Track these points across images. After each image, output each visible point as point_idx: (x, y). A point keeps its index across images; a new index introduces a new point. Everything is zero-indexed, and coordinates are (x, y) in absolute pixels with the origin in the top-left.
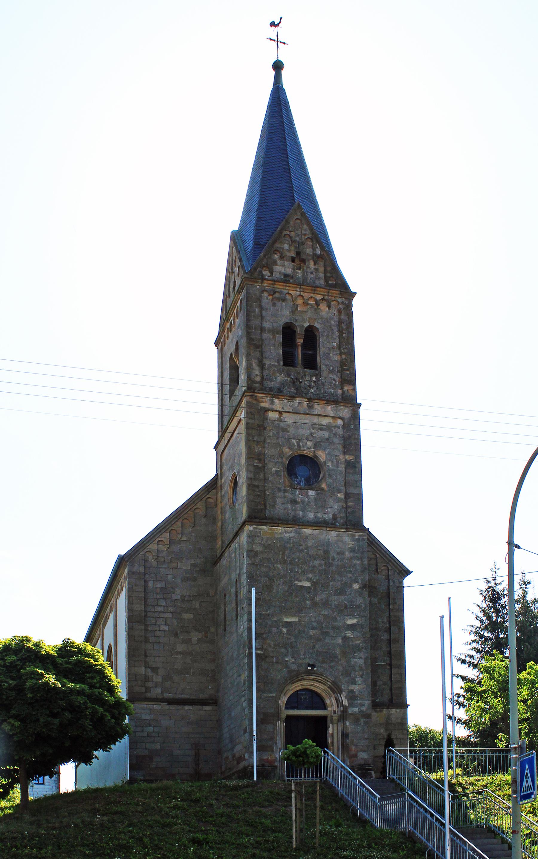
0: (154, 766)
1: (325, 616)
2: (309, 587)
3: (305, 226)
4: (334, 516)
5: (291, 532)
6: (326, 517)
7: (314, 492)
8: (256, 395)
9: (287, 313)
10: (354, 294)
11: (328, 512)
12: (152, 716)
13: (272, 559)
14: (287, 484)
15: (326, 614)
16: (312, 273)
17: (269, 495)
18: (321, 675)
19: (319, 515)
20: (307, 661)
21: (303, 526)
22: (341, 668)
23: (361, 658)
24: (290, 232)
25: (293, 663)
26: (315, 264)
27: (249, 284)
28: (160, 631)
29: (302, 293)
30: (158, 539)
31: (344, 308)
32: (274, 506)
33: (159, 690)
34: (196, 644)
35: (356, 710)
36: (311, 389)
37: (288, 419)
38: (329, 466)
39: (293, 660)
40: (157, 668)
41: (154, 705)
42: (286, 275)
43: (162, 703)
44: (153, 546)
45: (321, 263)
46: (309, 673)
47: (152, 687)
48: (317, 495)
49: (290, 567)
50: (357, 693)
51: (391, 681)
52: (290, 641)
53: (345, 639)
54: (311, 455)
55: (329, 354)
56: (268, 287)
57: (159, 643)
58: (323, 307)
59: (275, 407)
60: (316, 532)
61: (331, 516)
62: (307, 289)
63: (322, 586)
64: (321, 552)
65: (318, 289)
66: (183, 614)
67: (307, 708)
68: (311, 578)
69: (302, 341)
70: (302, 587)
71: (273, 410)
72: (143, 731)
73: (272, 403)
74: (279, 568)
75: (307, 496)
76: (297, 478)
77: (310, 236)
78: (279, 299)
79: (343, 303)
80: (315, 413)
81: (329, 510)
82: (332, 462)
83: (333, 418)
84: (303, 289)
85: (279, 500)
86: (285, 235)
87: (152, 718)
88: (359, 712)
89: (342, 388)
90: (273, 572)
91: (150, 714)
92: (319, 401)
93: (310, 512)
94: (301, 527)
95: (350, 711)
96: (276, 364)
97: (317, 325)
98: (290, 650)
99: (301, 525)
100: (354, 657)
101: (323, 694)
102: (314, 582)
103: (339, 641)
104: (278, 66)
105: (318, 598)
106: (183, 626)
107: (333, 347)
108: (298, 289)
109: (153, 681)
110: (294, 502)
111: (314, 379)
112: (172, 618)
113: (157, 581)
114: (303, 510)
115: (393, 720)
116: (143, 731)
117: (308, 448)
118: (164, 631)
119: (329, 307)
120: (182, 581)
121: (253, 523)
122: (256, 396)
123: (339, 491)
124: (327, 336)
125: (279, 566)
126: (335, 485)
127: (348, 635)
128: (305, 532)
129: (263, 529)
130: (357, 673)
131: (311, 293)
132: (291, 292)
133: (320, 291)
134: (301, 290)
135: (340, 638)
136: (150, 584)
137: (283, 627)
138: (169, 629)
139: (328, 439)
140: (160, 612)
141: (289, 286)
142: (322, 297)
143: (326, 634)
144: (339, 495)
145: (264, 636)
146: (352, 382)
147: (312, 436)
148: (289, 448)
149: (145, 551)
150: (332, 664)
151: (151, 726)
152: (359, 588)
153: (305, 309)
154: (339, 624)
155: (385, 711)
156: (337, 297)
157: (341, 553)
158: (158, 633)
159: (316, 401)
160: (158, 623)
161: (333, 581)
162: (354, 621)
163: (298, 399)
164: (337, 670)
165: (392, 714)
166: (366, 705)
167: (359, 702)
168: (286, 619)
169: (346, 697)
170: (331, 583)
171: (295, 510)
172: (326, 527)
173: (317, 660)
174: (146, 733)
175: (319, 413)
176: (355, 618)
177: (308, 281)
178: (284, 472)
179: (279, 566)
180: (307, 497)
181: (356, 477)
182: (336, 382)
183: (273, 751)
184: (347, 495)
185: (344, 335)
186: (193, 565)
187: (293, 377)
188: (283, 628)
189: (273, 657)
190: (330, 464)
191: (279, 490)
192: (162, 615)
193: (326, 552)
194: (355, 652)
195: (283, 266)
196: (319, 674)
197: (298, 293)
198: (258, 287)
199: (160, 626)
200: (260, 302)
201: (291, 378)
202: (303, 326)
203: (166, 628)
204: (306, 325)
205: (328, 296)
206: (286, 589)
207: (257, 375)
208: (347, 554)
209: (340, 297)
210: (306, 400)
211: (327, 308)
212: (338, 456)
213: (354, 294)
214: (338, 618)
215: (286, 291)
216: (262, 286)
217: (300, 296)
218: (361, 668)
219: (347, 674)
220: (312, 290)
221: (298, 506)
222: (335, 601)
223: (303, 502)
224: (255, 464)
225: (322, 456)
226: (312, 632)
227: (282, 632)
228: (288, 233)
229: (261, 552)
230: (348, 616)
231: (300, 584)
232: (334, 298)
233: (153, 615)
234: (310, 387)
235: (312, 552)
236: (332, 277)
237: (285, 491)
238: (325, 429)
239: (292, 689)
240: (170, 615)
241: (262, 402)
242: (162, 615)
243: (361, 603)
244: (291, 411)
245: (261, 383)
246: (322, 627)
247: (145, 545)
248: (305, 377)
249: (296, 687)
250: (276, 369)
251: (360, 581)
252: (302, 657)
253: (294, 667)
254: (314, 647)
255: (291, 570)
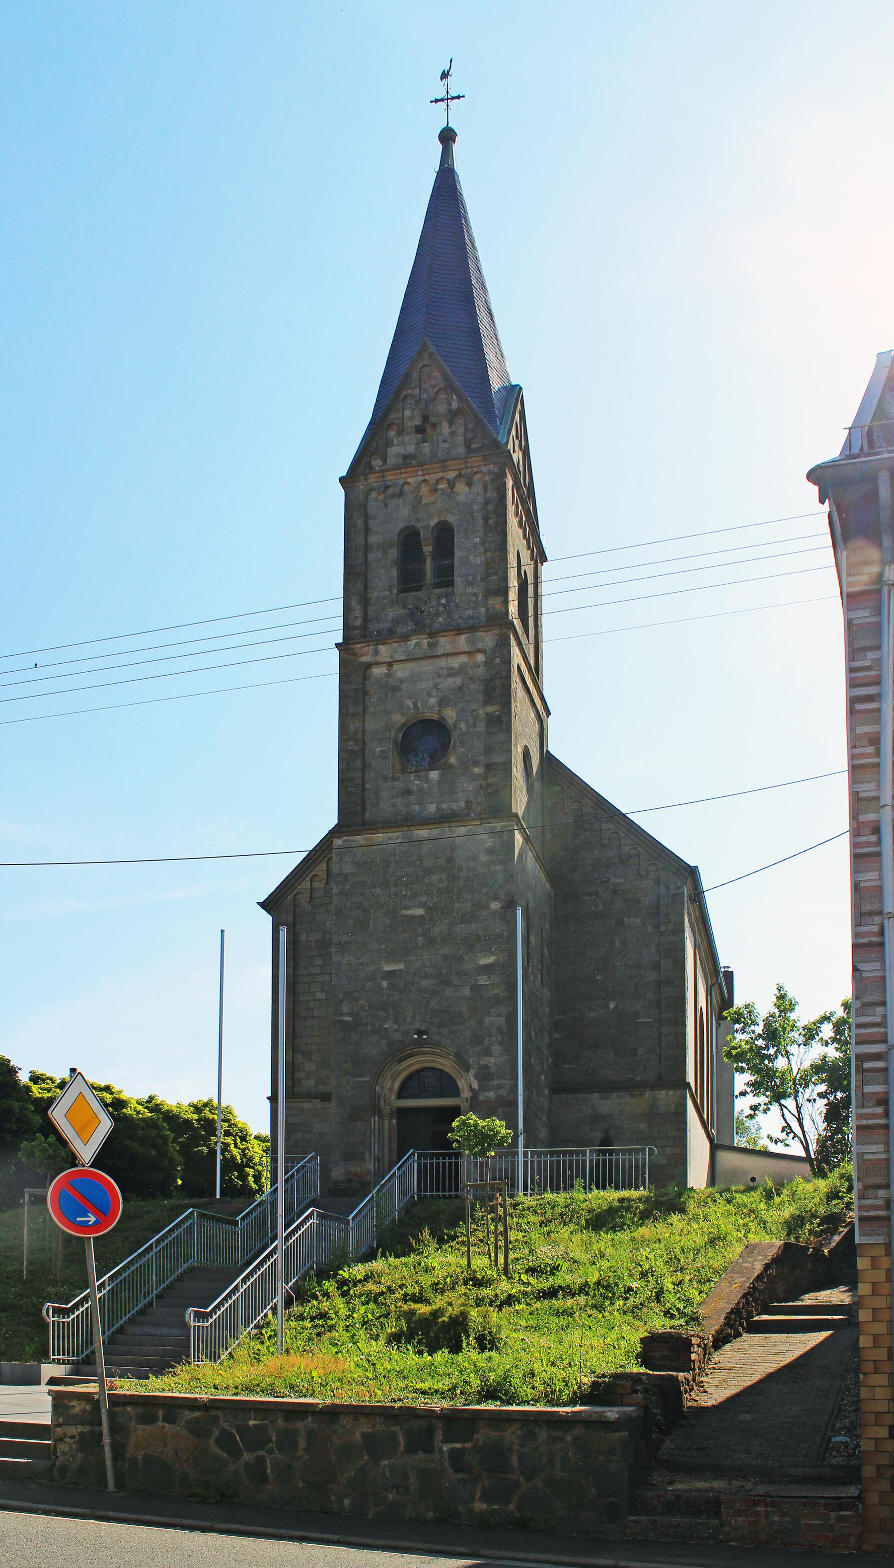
1: (445, 957)
2: (423, 916)
3: (435, 374)
4: (468, 803)
5: (398, 838)
6: (455, 806)
7: (437, 772)
8: (353, 646)
9: (405, 512)
11: (458, 798)
13: (369, 882)
14: (396, 769)
15: (447, 953)
16: (445, 441)
17: (370, 789)
18: (438, 1045)
19: (444, 806)
20: (417, 1025)
21: (413, 826)
22: (468, 1034)
23: (499, 1015)
24: (413, 389)
25: (396, 1030)
26: (451, 426)
28: (314, 1000)
29: (426, 477)
30: (312, 874)
31: (492, 480)
32: (376, 805)
33: (312, 1082)
35: (492, 1095)
36: (437, 617)
37: (401, 671)
38: (461, 729)
39: (396, 1027)
40: (310, 1052)
41: (303, 1102)
42: (405, 457)
44: (305, 885)
45: (460, 421)
46: (420, 1043)
48: (442, 776)
49: (394, 890)
50: (493, 1070)
51: (660, 1047)
52: (391, 999)
53: (476, 988)
54: (436, 717)
55: (468, 557)
57: (313, 1017)
58: (461, 488)
59: (380, 659)
60: (435, 832)
61: (462, 804)
63: (442, 912)
64: (442, 861)
65: (450, 463)
67: (433, 1096)
68: (426, 903)
69: (430, 548)
70: (412, 917)
71: (378, 664)
73: (377, 652)
74: (378, 894)
75: (427, 780)
76: (417, 756)
77: (442, 385)
78: (393, 496)
79: (489, 472)
80: (440, 653)
81: (460, 795)
82: (467, 723)
83: (468, 653)
84: (426, 469)
85: (384, 795)
86: (405, 397)
87: (301, 1121)
88: (496, 1098)
89: (485, 604)
90: (369, 901)
92: (444, 634)
93: (431, 803)
94: (411, 828)
95: (481, 1098)
96: (387, 593)
97: (451, 519)
98: (391, 1012)
99: (411, 826)
100: (489, 1015)
101: (453, 1074)
102: (431, 908)
103: (467, 992)
104: (447, 137)
105: (436, 931)
107: (475, 546)
108: (420, 473)
110: (407, 792)
111: (443, 601)
114: (420, 803)
115: (662, 1108)
117: (430, 708)
118: (320, 1000)
119: (470, 484)
121: (341, 835)
123: (476, 763)
124: (466, 531)
125: (378, 891)
126: (470, 755)
127: (481, 982)
128: (417, 834)
130: (494, 1039)
132: (409, 480)
134: (425, 472)
135: (468, 987)
136: (303, 937)
137: (383, 978)
138: (326, 996)
139: (460, 688)
141: (405, 473)
142: (456, 473)
143: (448, 983)
144: (476, 770)
145: (355, 995)
147: (437, 689)
148: (402, 714)
149: (295, 892)
150: (455, 1028)
152: (501, 908)
153: (432, 499)
154: (466, 967)
155: (648, 1094)
156: (479, 466)
157: (475, 858)
158: (311, 1004)
159: (441, 634)
160: (312, 990)
161: (459, 902)
162: (492, 959)
163: (414, 638)
164: (461, 1036)
165: (659, 1099)
166: (507, 1087)
167: (495, 1082)
168: (387, 968)
169: (475, 1077)
170: (456, 906)
171: (409, 804)
172: (450, 822)
173: (430, 1023)
175: (447, 652)
176: (493, 954)
177: (439, 454)
178: (393, 750)
179: (378, 891)
180: (426, 783)
181: (502, 737)
182: (477, 598)
183: (364, 1160)
184: (489, 768)
185: (490, 522)
187: (411, 607)
188: (382, 980)
189: (366, 1025)
190: (463, 726)
191: (385, 778)
193: (450, 860)
194: (491, 1007)
195: (402, 444)
196: (435, 1045)
197: (421, 478)
198: (361, 487)
199: (314, 994)
200: (366, 508)
201: (409, 609)
202: (428, 525)
203: (322, 996)
204: (433, 522)
205: (466, 468)
206: (388, 922)
207: (357, 617)
208: (483, 858)
209: (486, 465)
210: (426, 636)
212: (477, 710)
214: (466, 958)
215: (402, 481)
216: (368, 484)
217: (425, 481)
218: (500, 1030)
219: (477, 1041)
221: (412, 798)
222: (461, 932)
223: (421, 790)
224: (349, 748)
225: (450, 715)
226: (425, 983)
227: (380, 987)
228: (410, 391)
229: (353, 874)
230: (480, 952)
231: (409, 913)
232: (475, 470)
233: (306, 979)
234: (437, 615)
235: (428, 863)
236: (475, 437)
237: (394, 779)
238: (458, 672)
239: (404, 1069)
241: (363, 655)
242: (318, 978)
243: (503, 930)
244: (403, 658)
245: (364, 627)
246: (441, 974)
247: (292, 885)
248: (430, 602)
249: (411, 1065)
250: (386, 601)
251: (502, 897)
252: (409, 1020)
253: (397, 1036)
254: (428, 1004)
255: (396, 894)
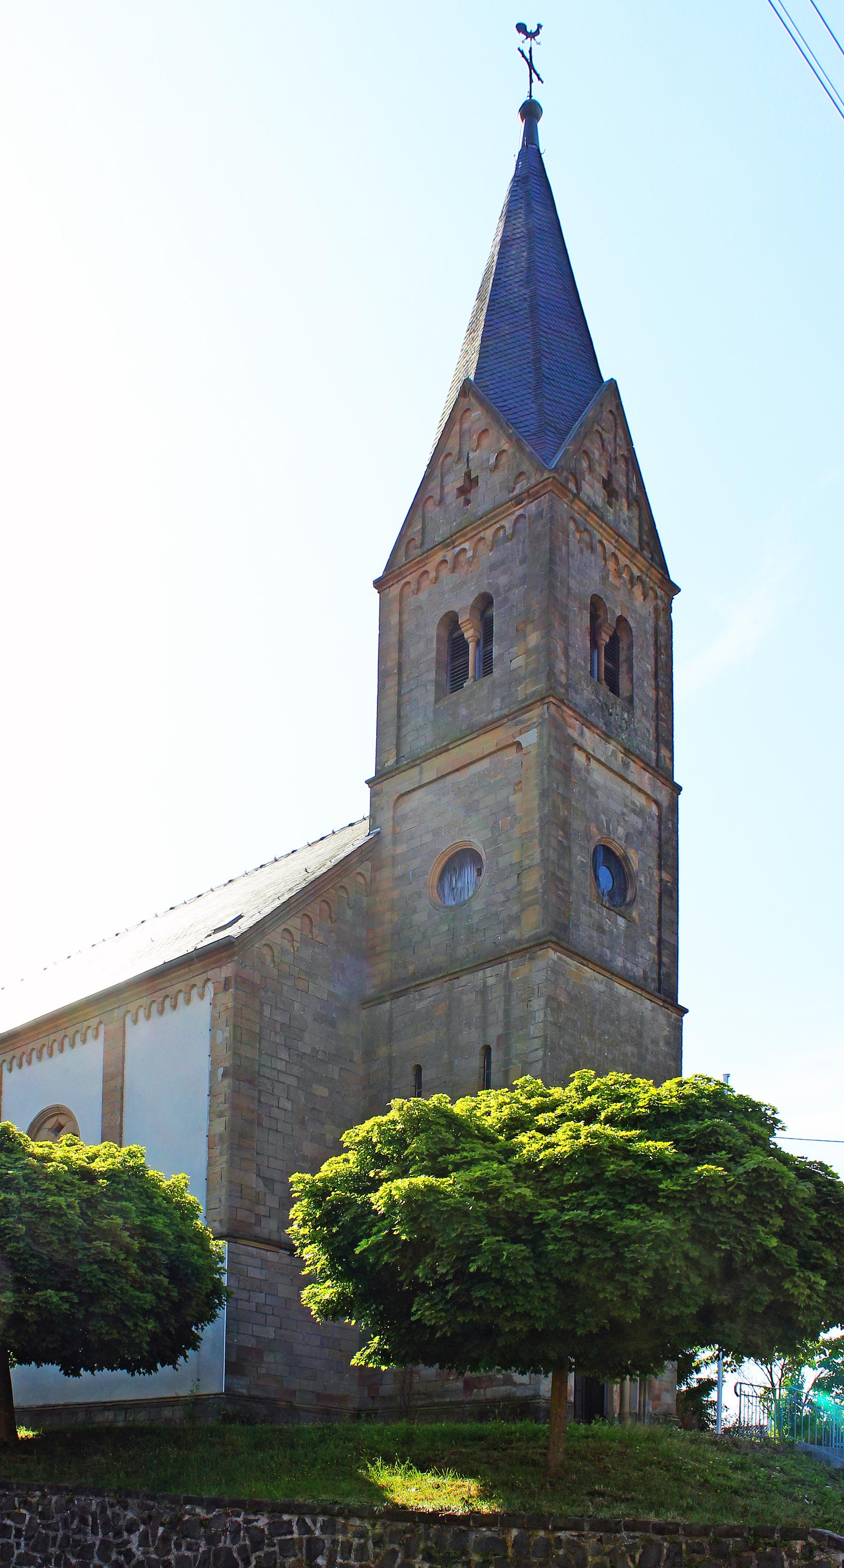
0: (263, 1371)
10: (676, 590)
12: (264, 1272)
19: (629, 965)
27: (555, 493)
34: (331, 1148)
41: (267, 1250)
43: (281, 1251)
47: (264, 1216)
56: (579, 514)
60: (630, 994)
62: (624, 547)
64: (634, 1032)
66: (314, 1086)
72: (248, 1301)
84: (620, 544)
91: (261, 1268)
106: (313, 1109)
109: (265, 1205)
111: (626, 716)
112: (298, 1088)
113: (277, 1008)
116: (248, 1301)
118: (285, 1110)
120: (315, 1020)
122: (562, 710)
129: (568, 964)
131: (627, 558)
133: (639, 561)
140: (279, 1071)
146: (670, 746)
151: (262, 1292)
157: (655, 1042)
158: (275, 1112)
174: (254, 1304)
186: (331, 994)
192: (282, 1078)
203: (288, 1105)
204: (618, 613)
211: (642, 598)
213: (676, 590)
220: (630, 553)
221: (605, 939)
240: (293, 1081)
